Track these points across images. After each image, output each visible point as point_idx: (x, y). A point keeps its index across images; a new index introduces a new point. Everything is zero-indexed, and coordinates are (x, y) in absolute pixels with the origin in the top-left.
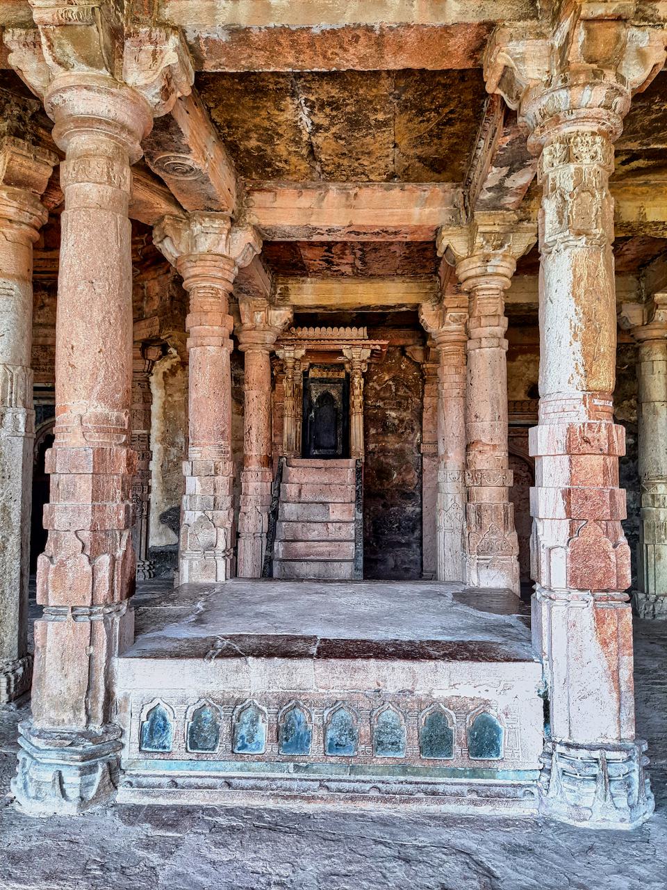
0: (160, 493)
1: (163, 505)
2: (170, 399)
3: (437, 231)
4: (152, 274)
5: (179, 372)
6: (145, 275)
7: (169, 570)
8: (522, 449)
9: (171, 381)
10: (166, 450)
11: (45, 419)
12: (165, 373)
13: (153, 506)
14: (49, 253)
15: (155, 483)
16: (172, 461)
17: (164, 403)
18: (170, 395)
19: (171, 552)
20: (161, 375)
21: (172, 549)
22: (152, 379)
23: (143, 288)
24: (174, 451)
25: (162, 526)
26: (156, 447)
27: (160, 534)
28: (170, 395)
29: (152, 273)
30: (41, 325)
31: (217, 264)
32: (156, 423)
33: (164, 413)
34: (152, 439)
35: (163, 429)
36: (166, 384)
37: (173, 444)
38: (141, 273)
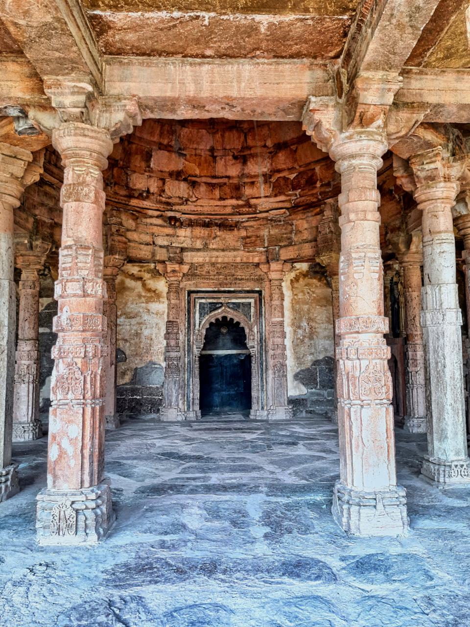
0: (292, 360)
1: (295, 368)
2: (296, 297)
3: (302, 104)
4: (300, 216)
5: (301, 279)
6: (293, 217)
7: (302, 411)
8: (256, 260)
9: (296, 285)
10: (295, 331)
11: (211, 312)
12: (291, 280)
13: (289, 368)
14: (222, 202)
15: (289, 353)
16: (299, 338)
17: (292, 300)
18: (296, 295)
19: (303, 400)
20: (289, 282)
21: (303, 397)
22: (283, 284)
23: (292, 225)
24: (300, 332)
25: (296, 382)
26: (288, 329)
27: (295, 388)
28: (296, 295)
29: (301, 215)
30: (214, 249)
31: (99, 135)
32: (287, 313)
33: (293, 307)
34: (286, 324)
35: (292, 317)
36: (293, 287)
37: (299, 327)
38: (290, 215)
